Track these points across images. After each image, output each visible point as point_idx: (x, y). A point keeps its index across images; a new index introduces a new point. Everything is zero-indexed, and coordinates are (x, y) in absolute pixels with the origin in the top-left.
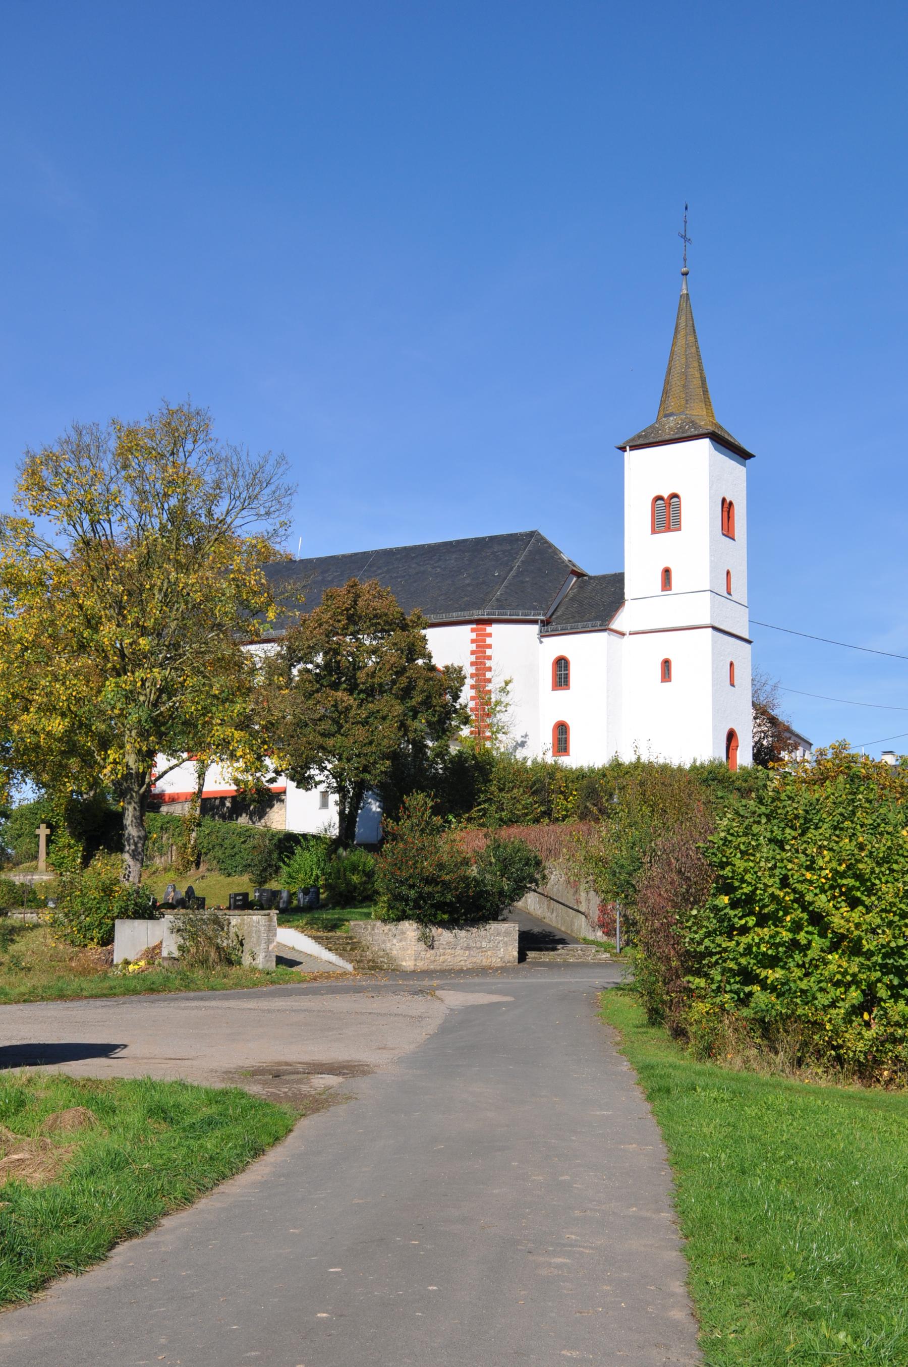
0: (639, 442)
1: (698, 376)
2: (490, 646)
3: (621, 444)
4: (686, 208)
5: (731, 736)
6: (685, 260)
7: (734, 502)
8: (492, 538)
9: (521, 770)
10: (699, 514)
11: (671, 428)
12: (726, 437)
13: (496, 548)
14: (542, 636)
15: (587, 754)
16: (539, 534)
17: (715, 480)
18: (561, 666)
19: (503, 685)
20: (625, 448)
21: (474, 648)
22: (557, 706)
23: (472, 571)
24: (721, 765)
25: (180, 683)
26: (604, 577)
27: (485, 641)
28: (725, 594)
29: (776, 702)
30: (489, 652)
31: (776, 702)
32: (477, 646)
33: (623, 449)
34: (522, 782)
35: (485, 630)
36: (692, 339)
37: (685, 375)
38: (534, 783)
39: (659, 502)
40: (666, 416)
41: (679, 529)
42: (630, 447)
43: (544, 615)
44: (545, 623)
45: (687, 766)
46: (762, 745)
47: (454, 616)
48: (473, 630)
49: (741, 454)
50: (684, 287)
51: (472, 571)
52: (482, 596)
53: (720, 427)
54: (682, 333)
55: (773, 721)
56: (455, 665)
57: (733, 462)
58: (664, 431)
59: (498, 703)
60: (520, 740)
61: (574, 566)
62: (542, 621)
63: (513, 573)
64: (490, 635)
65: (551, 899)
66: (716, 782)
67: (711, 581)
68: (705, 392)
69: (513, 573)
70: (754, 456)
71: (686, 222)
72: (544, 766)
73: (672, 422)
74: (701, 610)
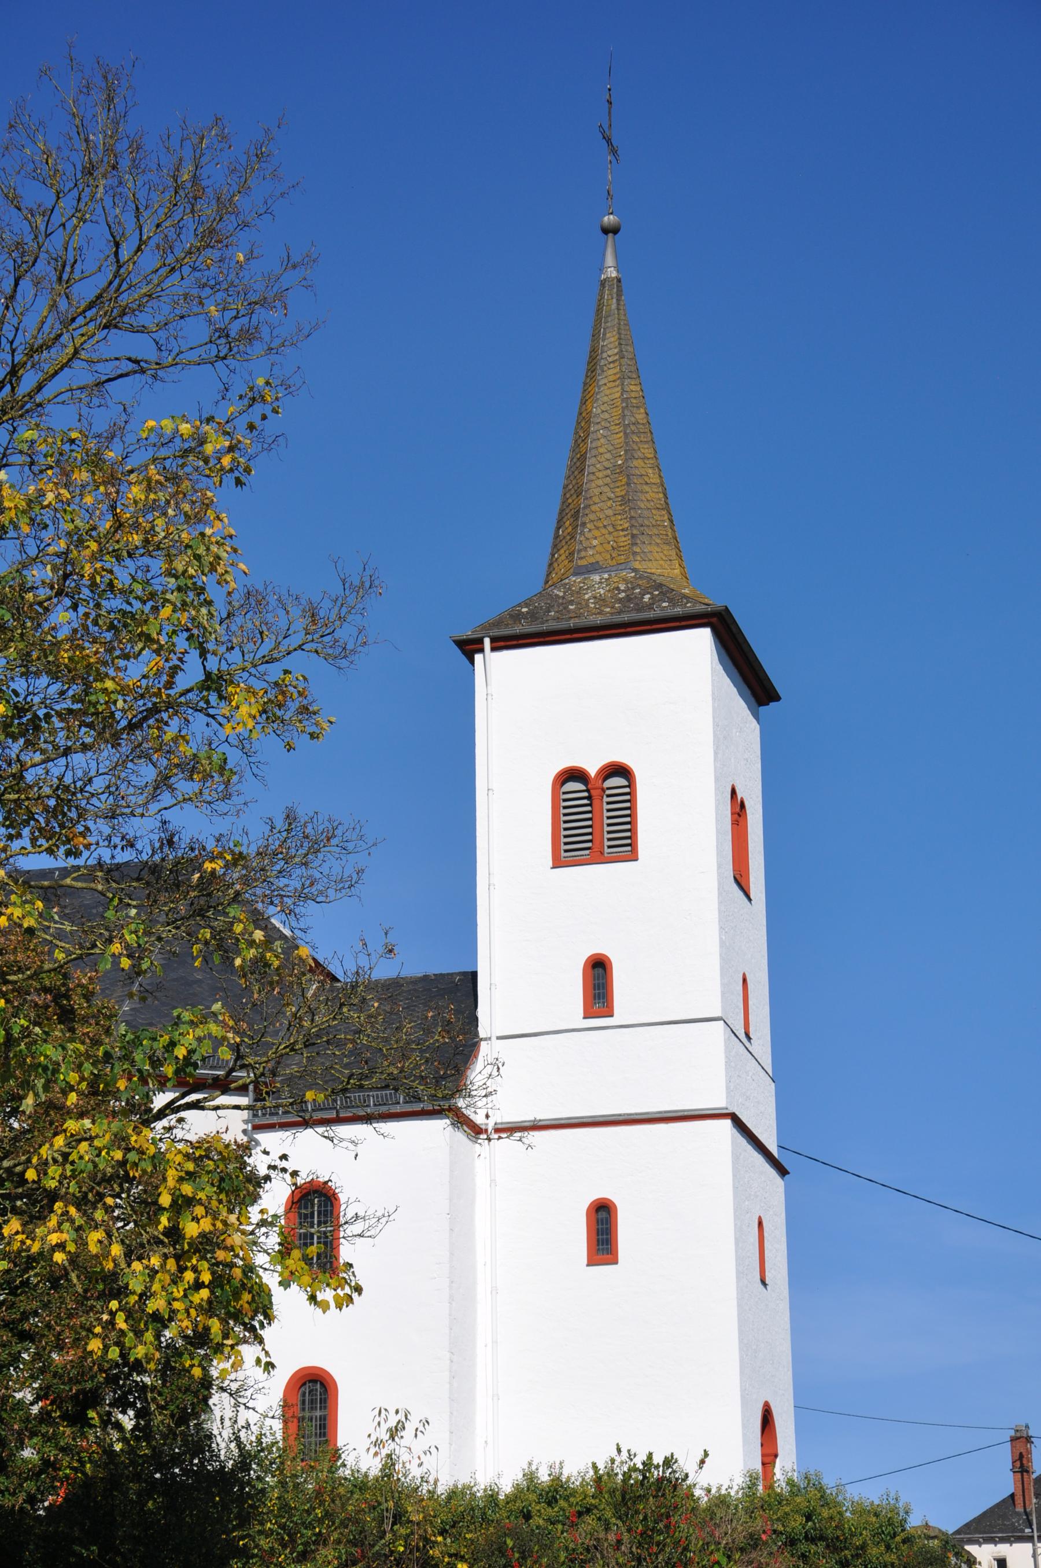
3: (467, 633)
11: (600, 600)
20: (480, 641)
25: (14, 775)
33: (470, 648)
37: (623, 472)
39: (572, 786)
42: (493, 640)
45: (506, 1488)
54: (612, 372)
66: (822, 1545)
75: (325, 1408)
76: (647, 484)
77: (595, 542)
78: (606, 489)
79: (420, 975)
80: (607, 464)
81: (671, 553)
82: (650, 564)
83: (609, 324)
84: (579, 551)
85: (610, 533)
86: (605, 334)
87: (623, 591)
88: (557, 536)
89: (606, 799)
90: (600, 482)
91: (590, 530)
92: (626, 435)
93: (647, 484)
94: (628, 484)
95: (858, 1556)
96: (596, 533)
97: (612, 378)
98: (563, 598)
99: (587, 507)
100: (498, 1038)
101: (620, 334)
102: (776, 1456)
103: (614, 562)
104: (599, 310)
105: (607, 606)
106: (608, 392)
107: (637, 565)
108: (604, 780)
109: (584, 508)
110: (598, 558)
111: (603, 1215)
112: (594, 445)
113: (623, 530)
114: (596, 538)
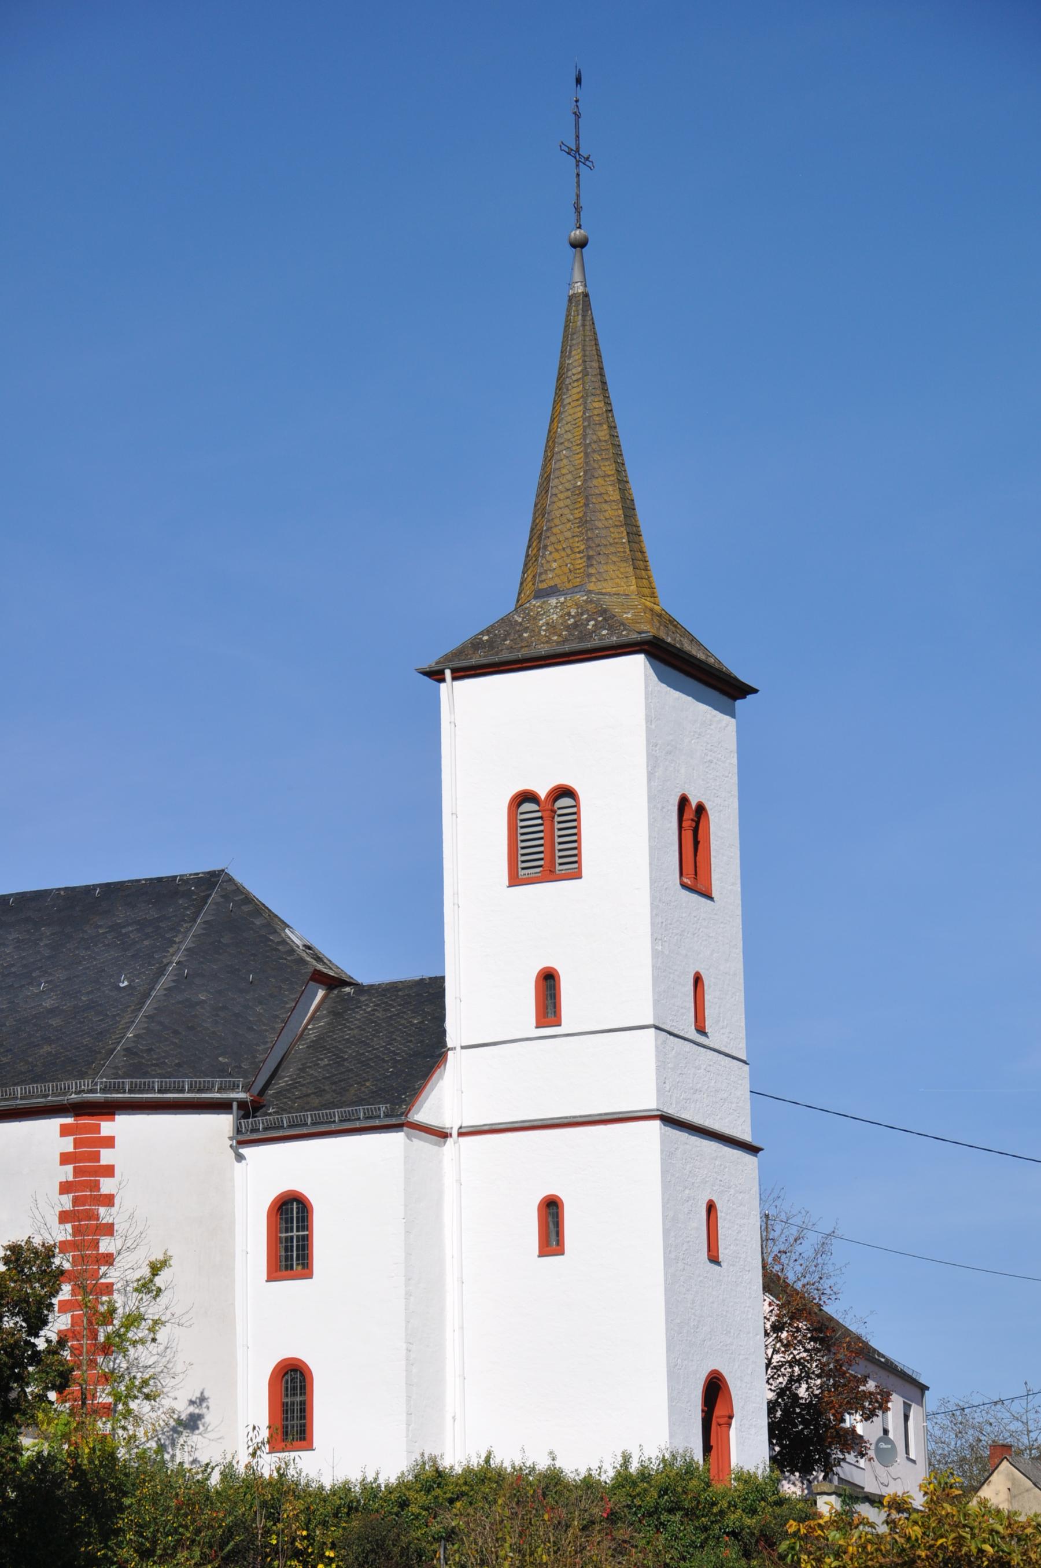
0: (476, 659)
1: (616, 496)
3: (429, 662)
4: (579, 81)
5: (715, 1390)
6: (578, 209)
7: (708, 806)
8: (111, 890)
9: (199, 1497)
10: (622, 838)
11: (551, 626)
12: (687, 647)
14: (242, 1143)
15: (354, 1450)
16: (231, 880)
17: (660, 752)
18: (291, 1216)
19: (146, 1271)
20: (442, 672)
21: (102, 1210)
22: (272, 1321)
23: (60, 975)
24: (690, 1470)
26: (392, 989)
27: (97, 1157)
28: (692, 1033)
29: (826, 1284)
31: (826, 1284)
32: (77, 1172)
33: (436, 675)
34: (198, 1532)
35: (97, 1129)
36: (598, 405)
37: (584, 495)
38: (230, 1532)
39: (527, 807)
40: (540, 594)
41: (577, 875)
42: (454, 671)
43: (247, 1089)
44: (247, 1110)
45: (608, 1476)
46: (796, 1397)
47: (20, 1095)
48: (65, 1131)
49: (722, 687)
50: (577, 276)
51: (60, 975)
52: (86, 1040)
53: (672, 621)
55: (826, 1333)
56: (37, 1241)
57: (703, 708)
58: (536, 633)
59: (134, 1320)
60: (184, 1410)
61: (319, 959)
62: (242, 1104)
63: (164, 981)
66: (679, 1514)
67: (656, 1003)
68: (634, 534)
69: (164, 981)
70: (755, 691)
71: (577, 116)
72: (252, 1483)
73: (553, 610)
74: (634, 1075)
75: (305, 1394)
76: (606, 502)
77: (554, 565)
78: (566, 511)
79: (418, 978)
80: (568, 486)
81: (627, 569)
82: (604, 584)
83: (574, 342)
84: (541, 574)
85: (568, 556)
86: (570, 352)
87: (573, 617)
88: (527, 556)
89: (557, 819)
90: (561, 504)
91: (551, 553)
92: (587, 455)
93: (606, 502)
94: (586, 505)
95: (716, 1522)
96: (556, 555)
97: (576, 397)
98: (521, 624)
99: (549, 529)
100: (463, 1048)
101: (584, 350)
102: (731, 1417)
103: (571, 585)
104: (567, 327)
105: (555, 634)
106: (571, 412)
107: (591, 587)
109: (547, 530)
110: (557, 581)
111: (553, 1210)
112: (557, 466)
113: (579, 552)
114: (555, 561)
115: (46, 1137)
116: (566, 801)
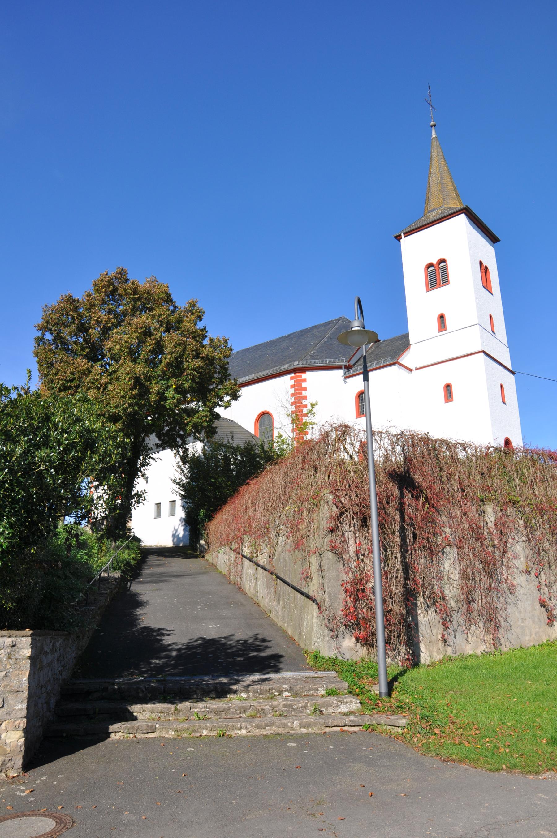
2: (305, 389)
13: (315, 331)
14: (346, 378)
20: (400, 235)
21: (303, 401)
27: (301, 385)
30: (304, 393)
33: (398, 238)
35: (301, 377)
37: (441, 184)
42: (404, 234)
48: (292, 378)
64: (305, 380)
65: (278, 577)
108: (439, 264)
111: (449, 388)
115: (286, 381)
116: (443, 264)
